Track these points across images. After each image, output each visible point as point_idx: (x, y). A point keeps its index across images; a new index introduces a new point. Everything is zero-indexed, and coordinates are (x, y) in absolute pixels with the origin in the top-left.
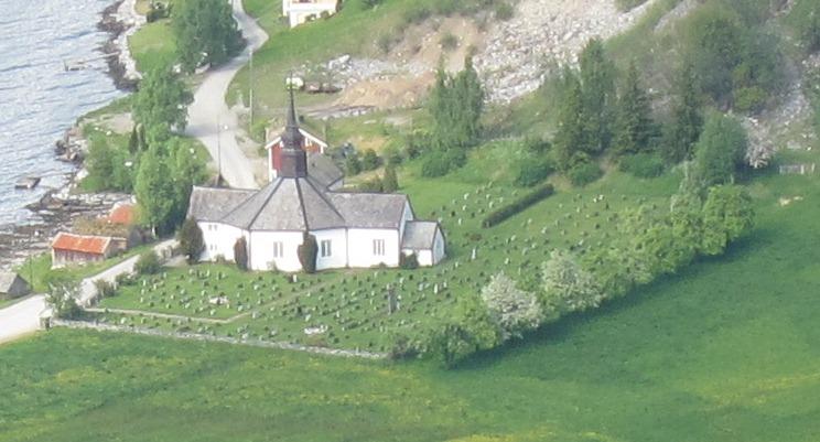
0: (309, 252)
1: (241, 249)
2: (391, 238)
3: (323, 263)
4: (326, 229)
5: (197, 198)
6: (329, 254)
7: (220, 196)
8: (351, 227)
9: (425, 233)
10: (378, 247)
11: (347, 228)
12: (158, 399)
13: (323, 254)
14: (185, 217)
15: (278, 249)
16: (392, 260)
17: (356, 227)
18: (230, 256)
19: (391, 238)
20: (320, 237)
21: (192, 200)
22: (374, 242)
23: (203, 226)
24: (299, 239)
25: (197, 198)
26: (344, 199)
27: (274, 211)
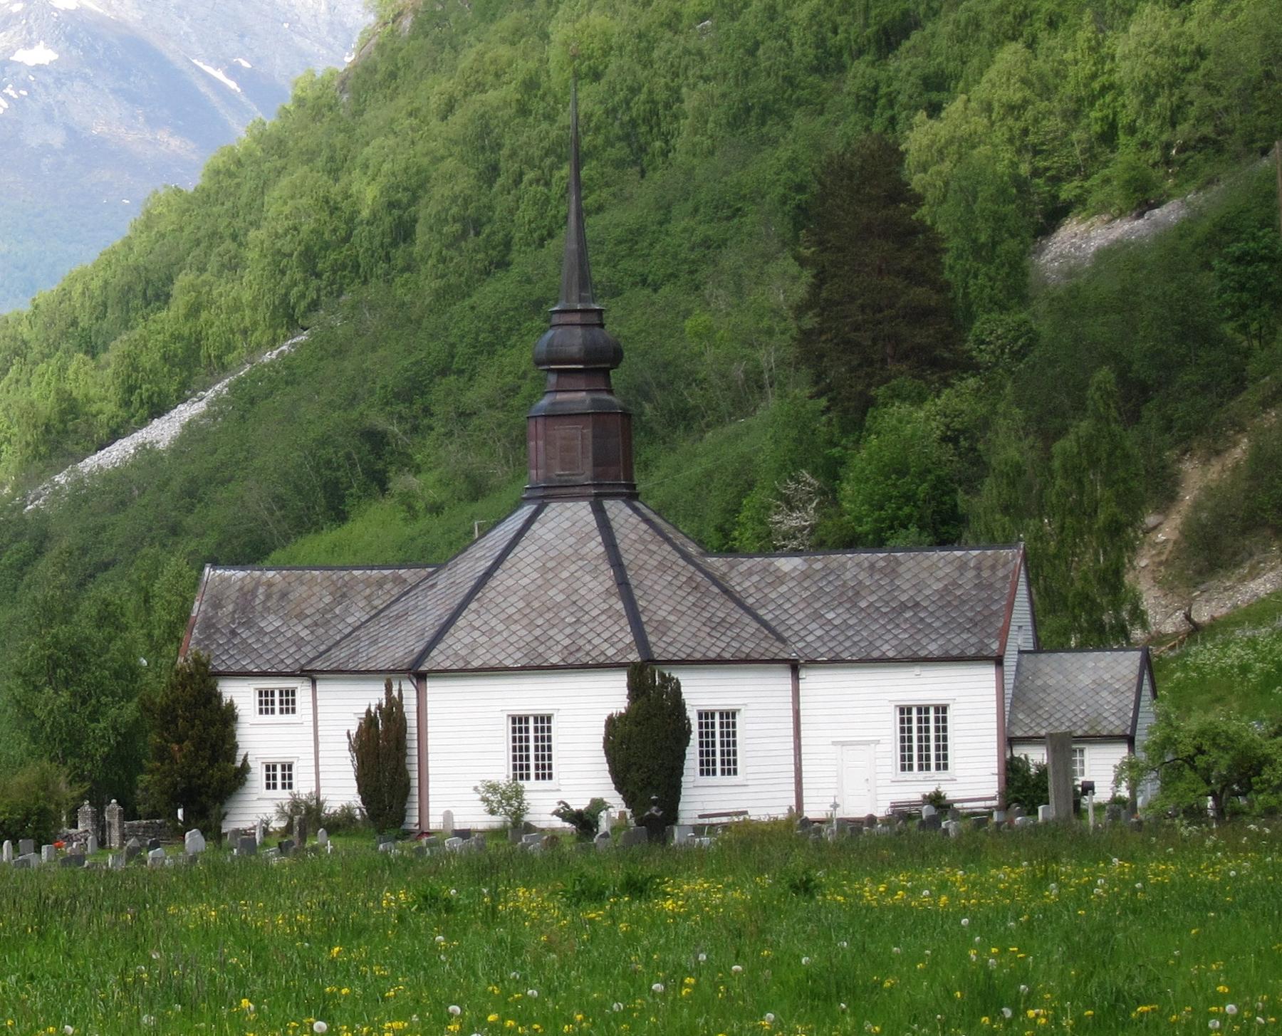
0: (651, 746)
1: (386, 755)
2: (971, 700)
3: (703, 797)
4: (718, 662)
5: (217, 604)
6: (730, 768)
7: (300, 591)
8: (813, 663)
9: (1100, 684)
10: (923, 735)
11: (795, 667)
12: (527, 510)
13: (707, 768)
14: (189, 615)
15: (531, 742)
16: (973, 776)
17: (835, 662)
18: (341, 790)
19: (971, 700)
20: (700, 692)
21: (197, 608)
22: (905, 711)
23: (240, 695)
24: (609, 695)
25: (217, 604)
26: (780, 579)
27: (514, 604)
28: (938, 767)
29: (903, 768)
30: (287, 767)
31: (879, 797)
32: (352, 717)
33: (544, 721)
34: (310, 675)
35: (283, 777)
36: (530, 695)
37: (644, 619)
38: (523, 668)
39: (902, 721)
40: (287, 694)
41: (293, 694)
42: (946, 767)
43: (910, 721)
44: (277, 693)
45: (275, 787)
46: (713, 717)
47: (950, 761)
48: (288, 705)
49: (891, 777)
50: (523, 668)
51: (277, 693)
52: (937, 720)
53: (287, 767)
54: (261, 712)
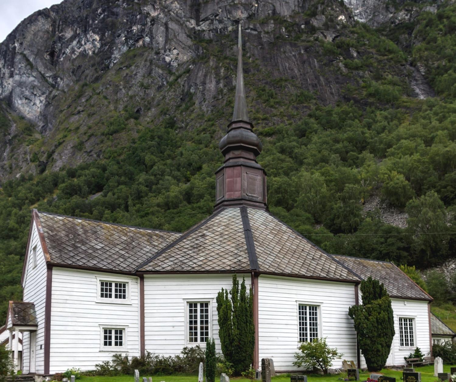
28: (116, 344)
29: (105, 344)
30: (119, 332)
31: (396, 357)
32: (182, 301)
33: (314, 308)
34: (140, 275)
35: (116, 338)
36: (309, 293)
37: (246, 247)
38: (311, 278)
39: (191, 311)
40: (120, 286)
41: (124, 286)
42: (121, 344)
43: (196, 311)
44: (113, 285)
45: (110, 344)
46: (306, 309)
47: (123, 341)
48: (121, 292)
49: (398, 348)
50: (311, 278)
51: (113, 285)
52: (202, 311)
53: (119, 332)
54: (102, 296)
